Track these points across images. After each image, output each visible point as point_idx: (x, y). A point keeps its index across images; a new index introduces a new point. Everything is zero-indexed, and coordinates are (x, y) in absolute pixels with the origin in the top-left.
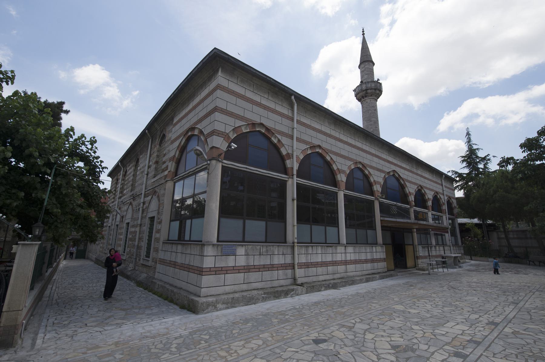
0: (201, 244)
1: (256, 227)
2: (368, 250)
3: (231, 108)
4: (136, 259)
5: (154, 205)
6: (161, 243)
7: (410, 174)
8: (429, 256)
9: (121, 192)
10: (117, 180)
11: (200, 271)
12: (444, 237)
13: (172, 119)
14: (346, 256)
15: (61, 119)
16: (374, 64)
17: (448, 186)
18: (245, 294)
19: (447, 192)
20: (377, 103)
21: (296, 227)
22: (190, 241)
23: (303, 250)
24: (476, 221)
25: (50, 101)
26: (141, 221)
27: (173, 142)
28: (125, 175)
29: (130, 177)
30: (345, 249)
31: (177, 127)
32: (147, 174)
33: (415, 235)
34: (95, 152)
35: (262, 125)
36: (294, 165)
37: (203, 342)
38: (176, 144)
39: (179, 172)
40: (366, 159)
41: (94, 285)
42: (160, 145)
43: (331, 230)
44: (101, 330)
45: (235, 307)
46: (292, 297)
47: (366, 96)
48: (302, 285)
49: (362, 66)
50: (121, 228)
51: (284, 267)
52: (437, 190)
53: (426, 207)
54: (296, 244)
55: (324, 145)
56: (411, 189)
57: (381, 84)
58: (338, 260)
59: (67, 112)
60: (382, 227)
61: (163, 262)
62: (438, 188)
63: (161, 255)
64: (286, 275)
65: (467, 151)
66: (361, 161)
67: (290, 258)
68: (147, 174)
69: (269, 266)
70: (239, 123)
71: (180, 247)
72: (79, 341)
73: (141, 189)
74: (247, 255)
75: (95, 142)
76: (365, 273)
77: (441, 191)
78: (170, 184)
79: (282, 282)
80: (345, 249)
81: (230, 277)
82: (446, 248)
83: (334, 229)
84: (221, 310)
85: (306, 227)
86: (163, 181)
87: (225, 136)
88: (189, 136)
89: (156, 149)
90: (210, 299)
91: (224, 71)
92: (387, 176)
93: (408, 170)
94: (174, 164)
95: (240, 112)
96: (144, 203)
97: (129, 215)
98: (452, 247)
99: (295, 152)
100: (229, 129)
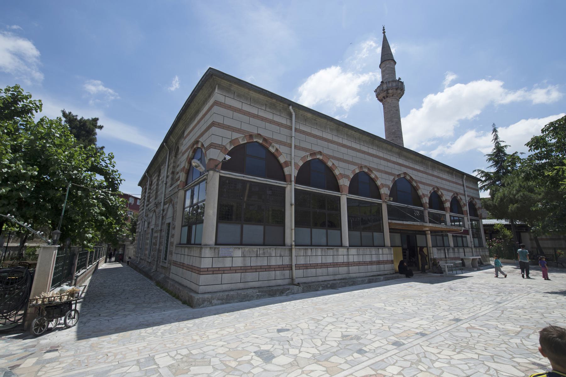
0: (200, 245)
1: (254, 231)
2: (374, 252)
3: (227, 122)
4: (157, 261)
5: (170, 213)
6: (174, 247)
7: (424, 175)
8: (446, 258)
9: (148, 201)
10: (146, 189)
11: (199, 271)
12: (464, 239)
13: (183, 132)
14: (348, 258)
15: (96, 134)
16: (395, 63)
17: (471, 186)
18: (239, 292)
19: (469, 192)
20: (400, 102)
21: (293, 231)
22: (194, 244)
23: (302, 253)
24: (503, 222)
25: (86, 118)
26: (161, 227)
27: (183, 154)
28: (151, 185)
29: (154, 187)
30: (348, 251)
31: (187, 139)
32: (166, 184)
33: (429, 237)
34: (114, 166)
35: (259, 135)
36: (292, 171)
37: (186, 329)
38: (186, 156)
39: (189, 182)
40: (372, 163)
41: (121, 284)
42: (176, 157)
43: (333, 233)
44: (109, 319)
45: (230, 303)
46: (287, 295)
47: (387, 97)
48: (298, 284)
49: (383, 65)
50: (148, 234)
51: (282, 268)
52: (457, 191)
53: (443, 209)
54: (293, 247)
55: (325, 151)
56: (425, 192)
57: (402, 83)
58: (339, 261)
59: (101, 127)
60: (390, 229)
61: (176, 264)
62: (459, 189)
63: (175, 258)
64: (284, 275)
65: (494, 149)
66: (367, 164)
67: (288, 259)
68: (166, 184)
69: (266, 267)
70: (236, 135)
71: (186, 249)
72: (89, 326)
73: (161, 198)
74: (244, 256)
75: (113, 157)
76: (369, 274)
77: (462, 192)
78: (181, 193)
79: (280, 282)
80: (348, 251)
81: (227, 277)
82: (467, 250)
83: (337, 232)
84: (216, 305)
85: (306, 231)
86: (177, 190)
87: (222, 148)
88: (195, 149)
89: (172, 161)
90: (206, 296)
91: (221, 88)
92: (396, 179)
93: (422, 172)
94: (184, 174)
95: (237, 125)
96: (163, 210)
97: (153, 222)
98: (473, 249)
99: (293, 160)
100: (226, 142)
